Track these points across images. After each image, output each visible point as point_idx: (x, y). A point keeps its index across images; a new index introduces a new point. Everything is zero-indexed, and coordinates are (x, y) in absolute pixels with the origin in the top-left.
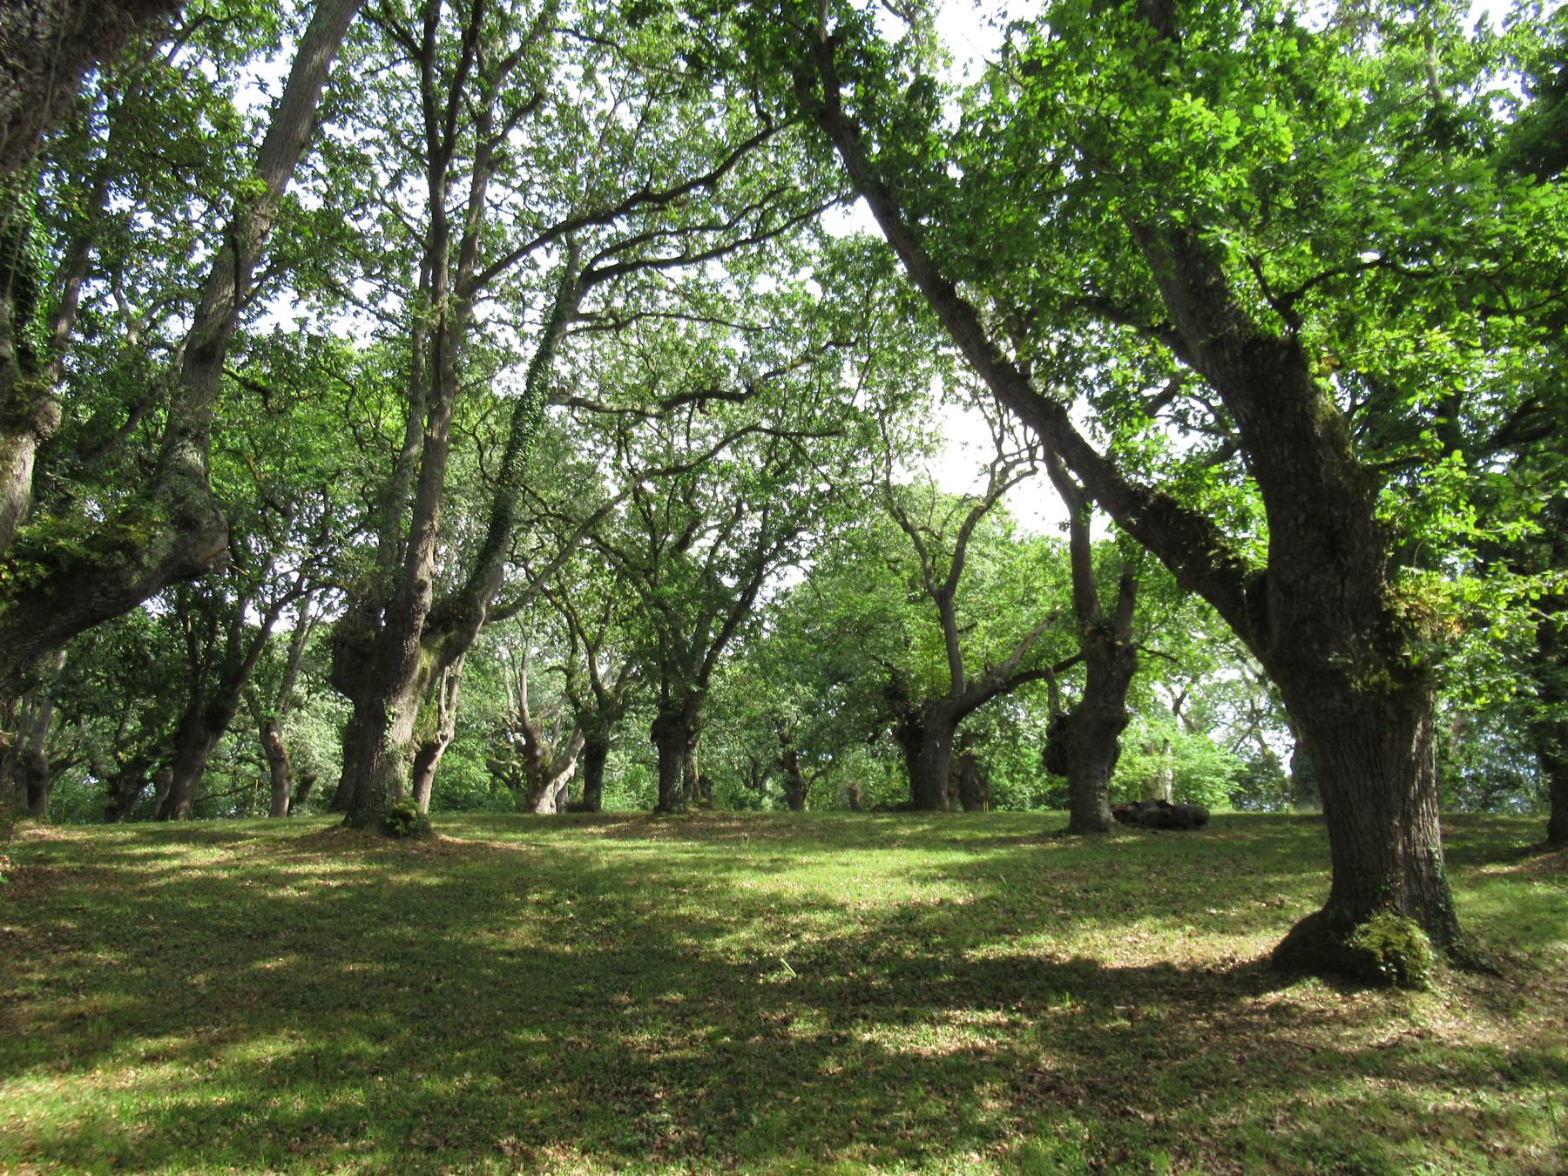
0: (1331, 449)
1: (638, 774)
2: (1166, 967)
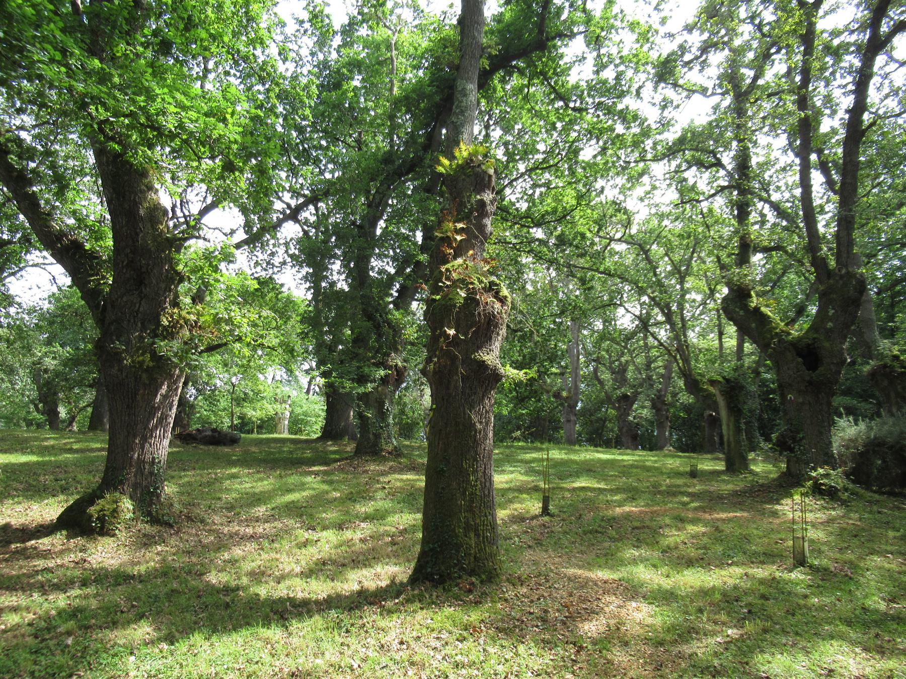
0: (149, 225)
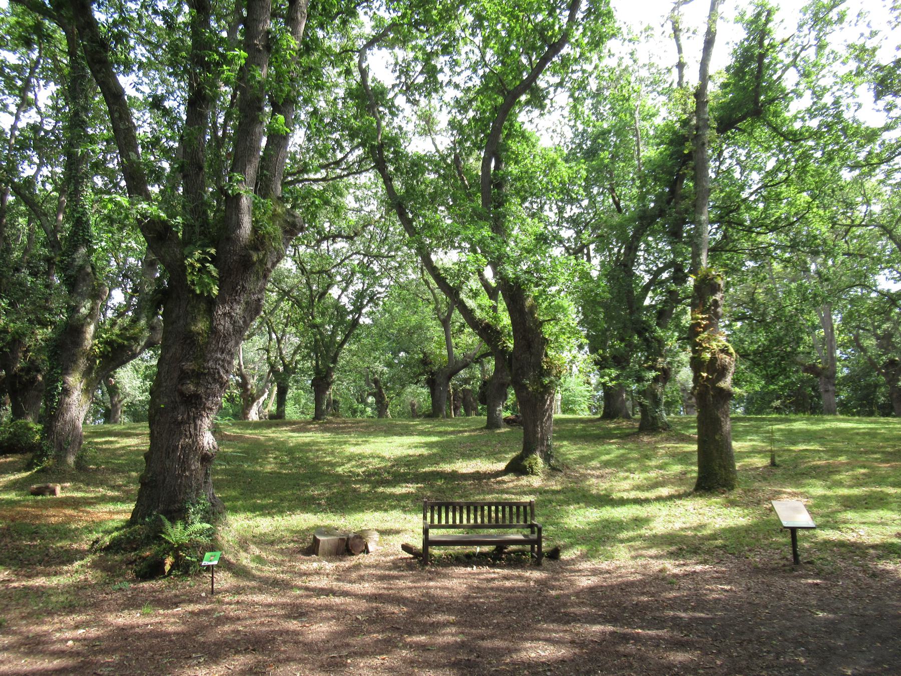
1: (299, 395)
2: (478, 472)
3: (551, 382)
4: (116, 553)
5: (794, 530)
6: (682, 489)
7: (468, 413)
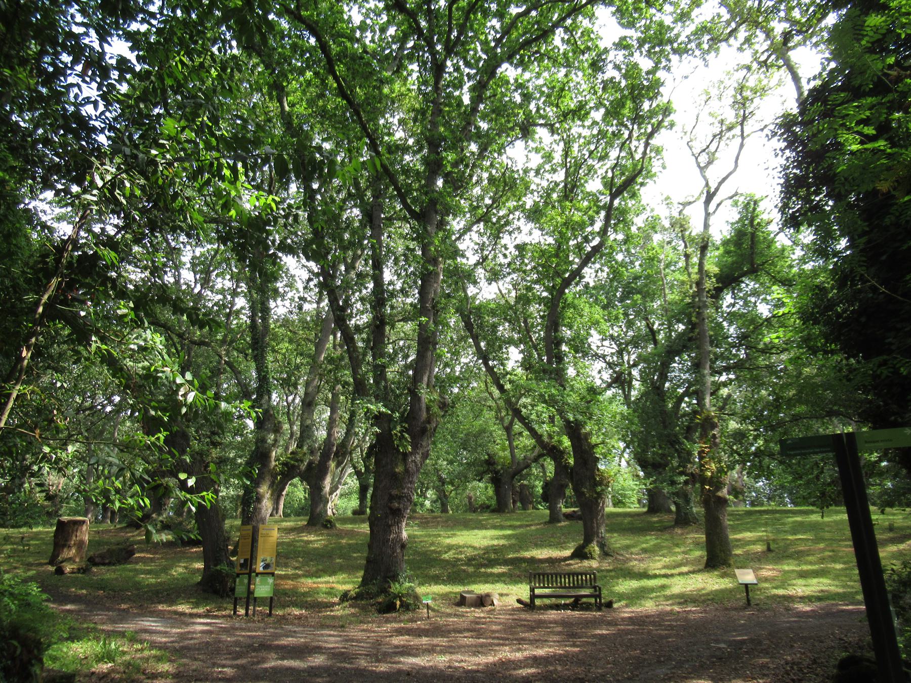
2: (550, 558)
3: (603, 490)
4: (362, 600)
5: (746, 585)
6: (696, 568)
7: (524, 508)
